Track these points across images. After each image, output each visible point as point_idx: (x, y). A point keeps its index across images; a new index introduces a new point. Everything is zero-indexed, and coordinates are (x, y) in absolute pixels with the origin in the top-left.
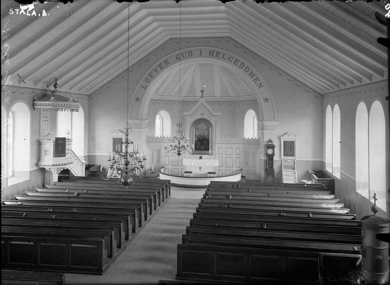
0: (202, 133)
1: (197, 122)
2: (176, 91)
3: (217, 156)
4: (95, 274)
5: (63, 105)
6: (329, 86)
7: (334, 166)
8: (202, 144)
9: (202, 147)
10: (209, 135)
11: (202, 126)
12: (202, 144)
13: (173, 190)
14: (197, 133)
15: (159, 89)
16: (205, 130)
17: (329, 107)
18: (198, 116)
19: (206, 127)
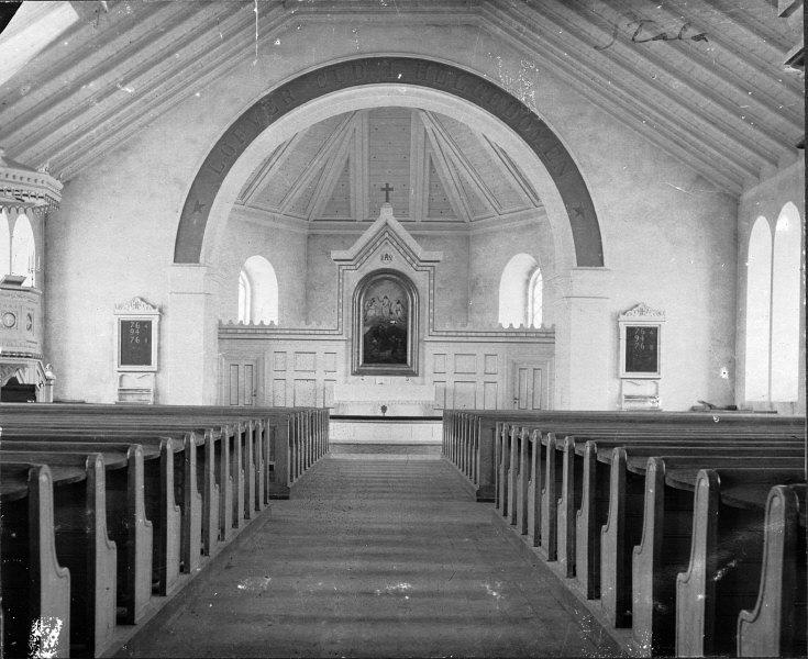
0: (386, 311)
1: (370, 282)
2: (297, 196)
3: (428, 380)
4: (181, 541)
5: (10, 178)
6: (355, 574)
7: (711, 48)
8: (384, 346)
9: (388, 353)
10: (406, 318)
11: (387, 293)
12: (384, 346)
13: (333, 425)
14: (371, 313)
15: (251, 186)
16: (394, 303)
17: (761, 223)
18: (375, 264)
19: (397, 294)
